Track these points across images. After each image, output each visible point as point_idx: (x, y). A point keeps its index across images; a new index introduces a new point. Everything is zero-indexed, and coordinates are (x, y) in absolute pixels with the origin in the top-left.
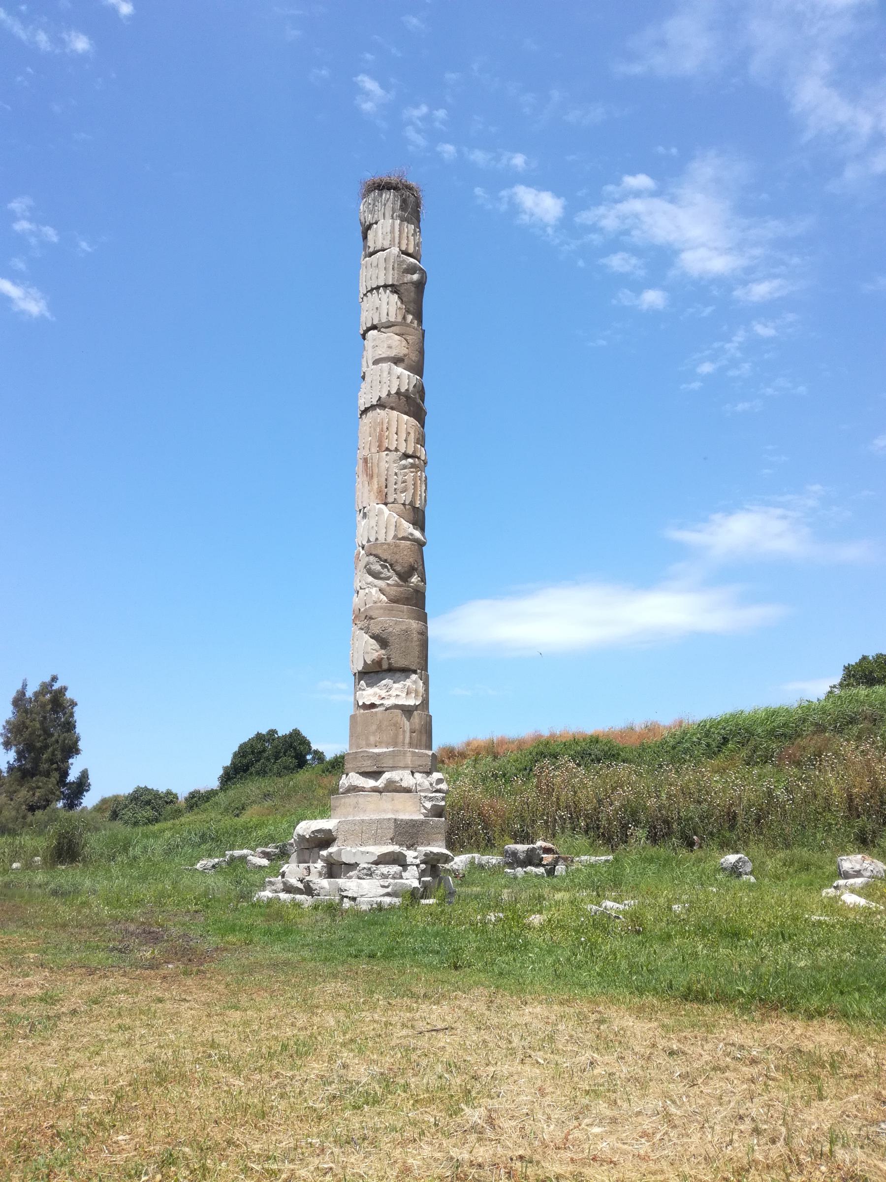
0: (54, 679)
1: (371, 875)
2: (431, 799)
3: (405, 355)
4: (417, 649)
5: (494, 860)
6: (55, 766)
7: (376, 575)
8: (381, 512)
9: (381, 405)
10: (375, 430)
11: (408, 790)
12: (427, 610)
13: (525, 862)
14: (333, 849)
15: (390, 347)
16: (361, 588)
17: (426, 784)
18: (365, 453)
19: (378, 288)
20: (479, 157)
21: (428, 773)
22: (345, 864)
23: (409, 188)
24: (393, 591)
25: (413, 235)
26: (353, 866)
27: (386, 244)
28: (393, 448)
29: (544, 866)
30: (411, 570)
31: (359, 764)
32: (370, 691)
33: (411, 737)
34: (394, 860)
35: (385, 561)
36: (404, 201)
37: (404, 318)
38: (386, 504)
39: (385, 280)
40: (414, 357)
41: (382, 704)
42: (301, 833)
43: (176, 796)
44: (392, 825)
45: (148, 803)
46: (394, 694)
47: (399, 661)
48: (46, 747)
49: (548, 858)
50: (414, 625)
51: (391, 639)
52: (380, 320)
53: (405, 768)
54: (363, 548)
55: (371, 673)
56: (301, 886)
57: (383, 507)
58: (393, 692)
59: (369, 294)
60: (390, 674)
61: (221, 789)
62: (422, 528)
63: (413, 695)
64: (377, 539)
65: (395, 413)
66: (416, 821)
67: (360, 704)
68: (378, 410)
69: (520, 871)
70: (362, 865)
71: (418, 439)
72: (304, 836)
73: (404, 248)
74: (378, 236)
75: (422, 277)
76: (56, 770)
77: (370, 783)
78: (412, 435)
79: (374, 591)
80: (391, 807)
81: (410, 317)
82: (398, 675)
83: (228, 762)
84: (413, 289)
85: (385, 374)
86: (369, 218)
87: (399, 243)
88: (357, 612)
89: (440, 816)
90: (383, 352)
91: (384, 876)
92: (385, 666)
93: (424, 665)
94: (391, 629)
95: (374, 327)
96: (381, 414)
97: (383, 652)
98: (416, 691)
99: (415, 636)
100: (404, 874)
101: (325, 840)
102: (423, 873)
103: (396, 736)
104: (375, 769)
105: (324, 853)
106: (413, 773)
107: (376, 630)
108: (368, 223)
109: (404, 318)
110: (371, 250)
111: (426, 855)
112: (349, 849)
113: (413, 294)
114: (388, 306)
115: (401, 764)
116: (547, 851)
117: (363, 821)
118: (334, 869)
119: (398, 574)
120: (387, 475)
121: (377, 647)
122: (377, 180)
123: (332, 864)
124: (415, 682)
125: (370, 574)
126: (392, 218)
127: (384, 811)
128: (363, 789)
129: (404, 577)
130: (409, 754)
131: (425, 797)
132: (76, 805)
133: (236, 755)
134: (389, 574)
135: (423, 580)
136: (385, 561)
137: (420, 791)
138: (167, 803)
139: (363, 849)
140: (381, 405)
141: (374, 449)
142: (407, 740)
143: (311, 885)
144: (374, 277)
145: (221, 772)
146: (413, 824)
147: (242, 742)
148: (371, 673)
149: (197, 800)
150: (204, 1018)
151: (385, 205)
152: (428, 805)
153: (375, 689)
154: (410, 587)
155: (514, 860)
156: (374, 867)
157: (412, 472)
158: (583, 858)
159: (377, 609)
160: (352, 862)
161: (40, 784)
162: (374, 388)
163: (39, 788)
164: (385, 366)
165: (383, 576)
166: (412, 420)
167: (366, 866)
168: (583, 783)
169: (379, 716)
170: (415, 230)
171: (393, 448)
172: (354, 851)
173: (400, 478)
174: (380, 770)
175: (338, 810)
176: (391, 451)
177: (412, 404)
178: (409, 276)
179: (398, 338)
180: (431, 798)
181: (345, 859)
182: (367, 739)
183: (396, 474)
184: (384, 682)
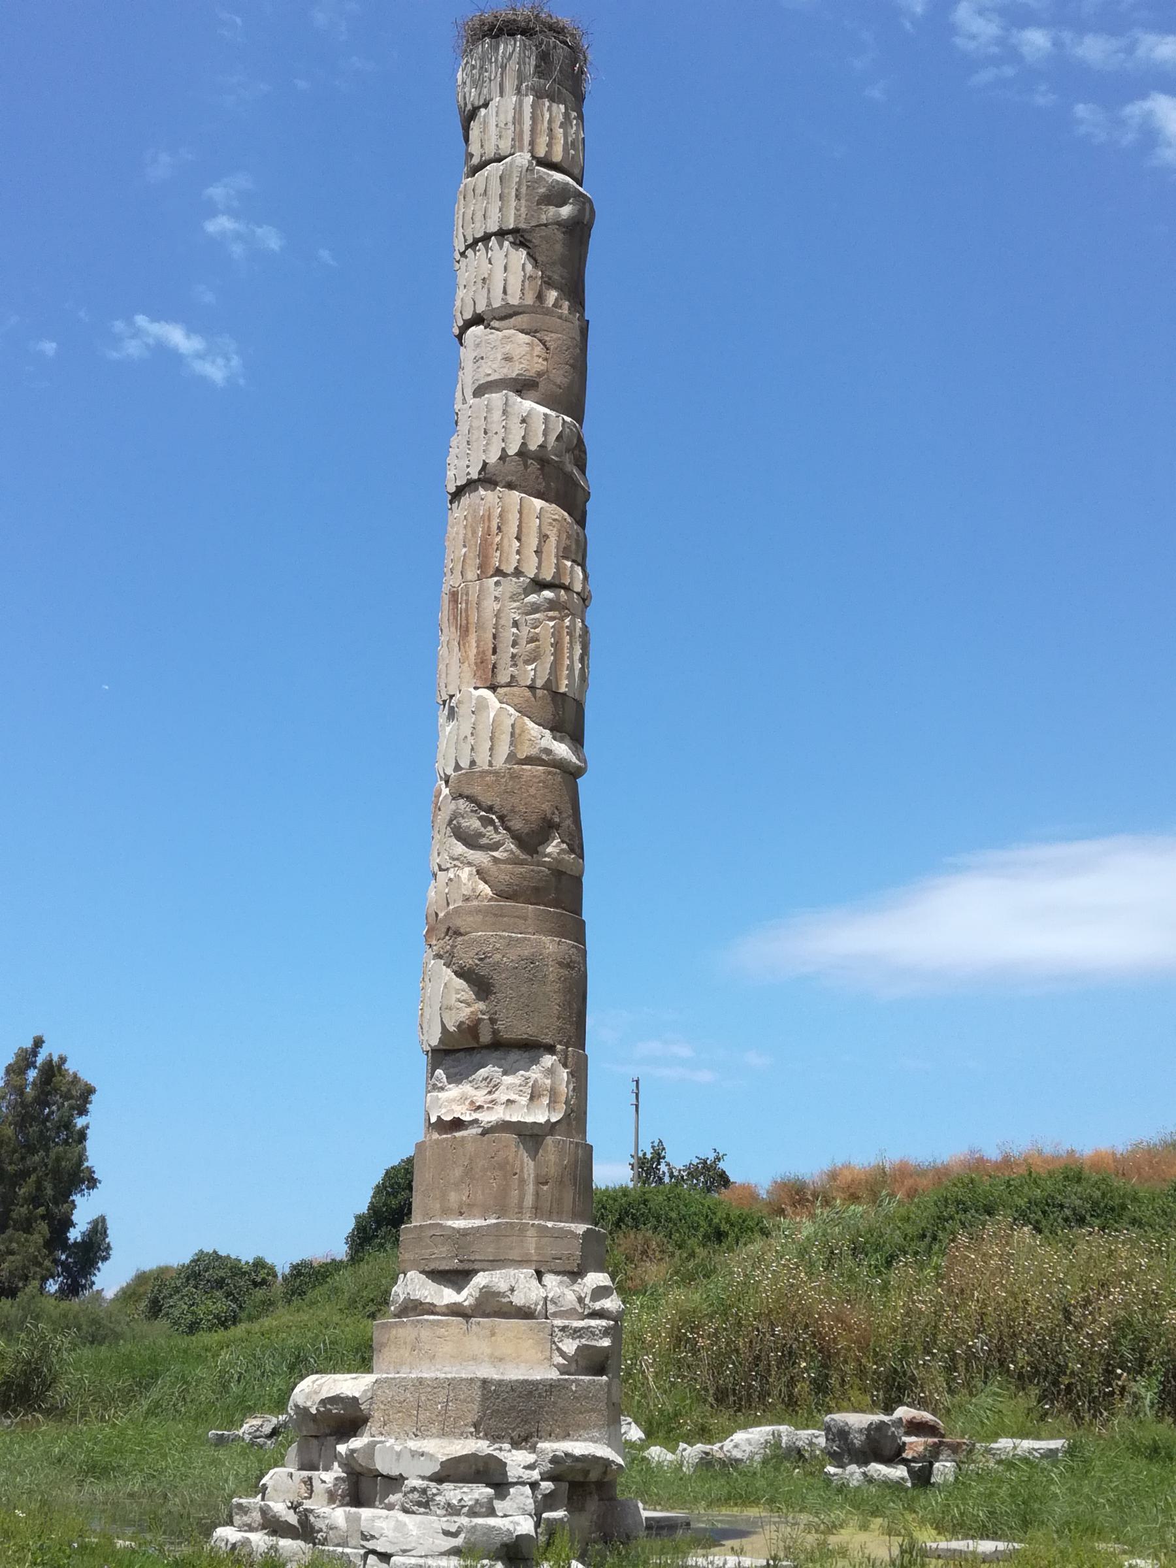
0: (38, 1043)
1: (426, 1505)
2: (576, 1333)
3: (540, 374)
4: (557, 999)
5: (812, 1437)
6: (41, 1210)
7: (470, 840)
8: (482, 705)
9: (487, 479)
10: (474, 532)
11: (525, 1313)
12: (589, 913)
13: (864, 1453)
15: (508, 359)
16: (441, 869)
17: (570, 1298)
18: (452, 581)
19: (486, 238)
20: (1093, 49)
21: (576, 1275)
22: (382, 1475)
23: (557, 30)
24: (504, 875)
25: (562, 125)
26: (395, 1482)
27: (505, 146)
28: (509, 569)
29: (905, 1462)
30: (546, 829)
31: (426, 1253)
32: (454, 1091)
33: (537, 1194)
34: (478, 1472)
35: (490, 809)
36: (544, 57)
37: (540, 297)
38: (493, 688)
39: (501, 220)
40: (560, 376)
41: (476, 1121)
42: (301, 1403)
43: (272, 1272)
44: (477, 1393)
45: (220, 1283)
46: (504, 1098)
47: (516, 1027)
48: (24, 1174)
49: (915, 1444)
50: (551, 946)
51: (498, 979)
52: (489, 304)
54: (447, 782)
55: (458, 1053)
56: (292, 1519)
58: (502, 1096)
59: (470, 252)
60: (497, 1054)
61: (352, 1258)
62: (576, 738)
63: (545, 1101)
64: (473, 763)
65: (516, 495)
66: (535, 1384)
67: (433, 1120)
68: (482, 492)
69: (854, 1472)
71: (566, 548)
72: (306, 1409)
73: (541, 152)
74: (491, 132)
75: (582, 211)
76: (43, 1217)
77: (448, 1296)
78: (553, 540)
79: (465, 873)
80: (488, 1351)
81: (552, 295)
82: (514, 1055)
83: (363, 1208)
84: (560, 236)
85: (497, 415)
86: (473, 95)
87: (532, 143)
88: (432, 919)
89: (601, 1371)
90: (494, 370)
91: (453, 1510)
92: (485, 1037)
93: (577, 1036)
94: (498, 957)
95: (477, 320)
96: (487, 497)
97: (481, 1005)
98: (553, 1093)
99: (552, 971)
100: (498, 1504)
101: (346, 1420)
102: (548, 1502)
103: (504, 1192)
104: (455, 1264)
105: (342, 1448)
106: (539, 1275)
107: (468, 959)
108: (469, 107)
109: (540, 297)
110: (475, 161)
111: (555, 1460)
112: (391, 1441)
113: (563, 249)
114: (507, 273)
115: (515, 1255)
116: (916, 1428)
117: (421, 1381)
118: (363, 1486)
119: (517, 838)
120: (496, 626)
121: (469, 995)
122: (488, 16)
123: (360, 1474)
124: (550, 1072)
125: (459, 838)
126: (518, 91)
127: (474, 1359)
128: (431, 1309)
129: (530, 842)
130: (531, 1232)
131: (563, 1329)
132: (84, 1287)
133: (379, 1190)
134: (497, 838)
135: (576, 846)
136: (490, 809)
137: (555, 1315)
138: (255, 1284)
139: (413, 1444)
140: (487, 479)
141: (471, 574)
142: (529, 1201)
143: (312, 1519)
144: (479, 216)
145: (350, 1225)
146: (528, 1390)
147: (388, 1166)
148: (458, 1053)
149: (307, 1278)
151: (504, 67)
152: (570, 1346)
153: (466, 1088)
154: (544, 864)
155: (846, 1449)
157: (551, 619)
158: (1004, 1443)
159: (470, 913)
160: (394, 1472)
161: (14, 1245)
162: (474, 445)
163: (12, 1253)
165: (484, 841)
166: (555, 511)
168: (1020, 1268)
169: (470, 1148)
170: (566, 115)
171: (509, 569)
172: (398, 1448)
173: (525, 632)
174: (467, 1266)
175: (385, 1350)
176: (505, 575)
177: (557, 475)
178: (552, 210)
179: (527, 338)
181: (383, 1465)
182: (444, 1197)
183: (516, 624)
184: (483, 1072)
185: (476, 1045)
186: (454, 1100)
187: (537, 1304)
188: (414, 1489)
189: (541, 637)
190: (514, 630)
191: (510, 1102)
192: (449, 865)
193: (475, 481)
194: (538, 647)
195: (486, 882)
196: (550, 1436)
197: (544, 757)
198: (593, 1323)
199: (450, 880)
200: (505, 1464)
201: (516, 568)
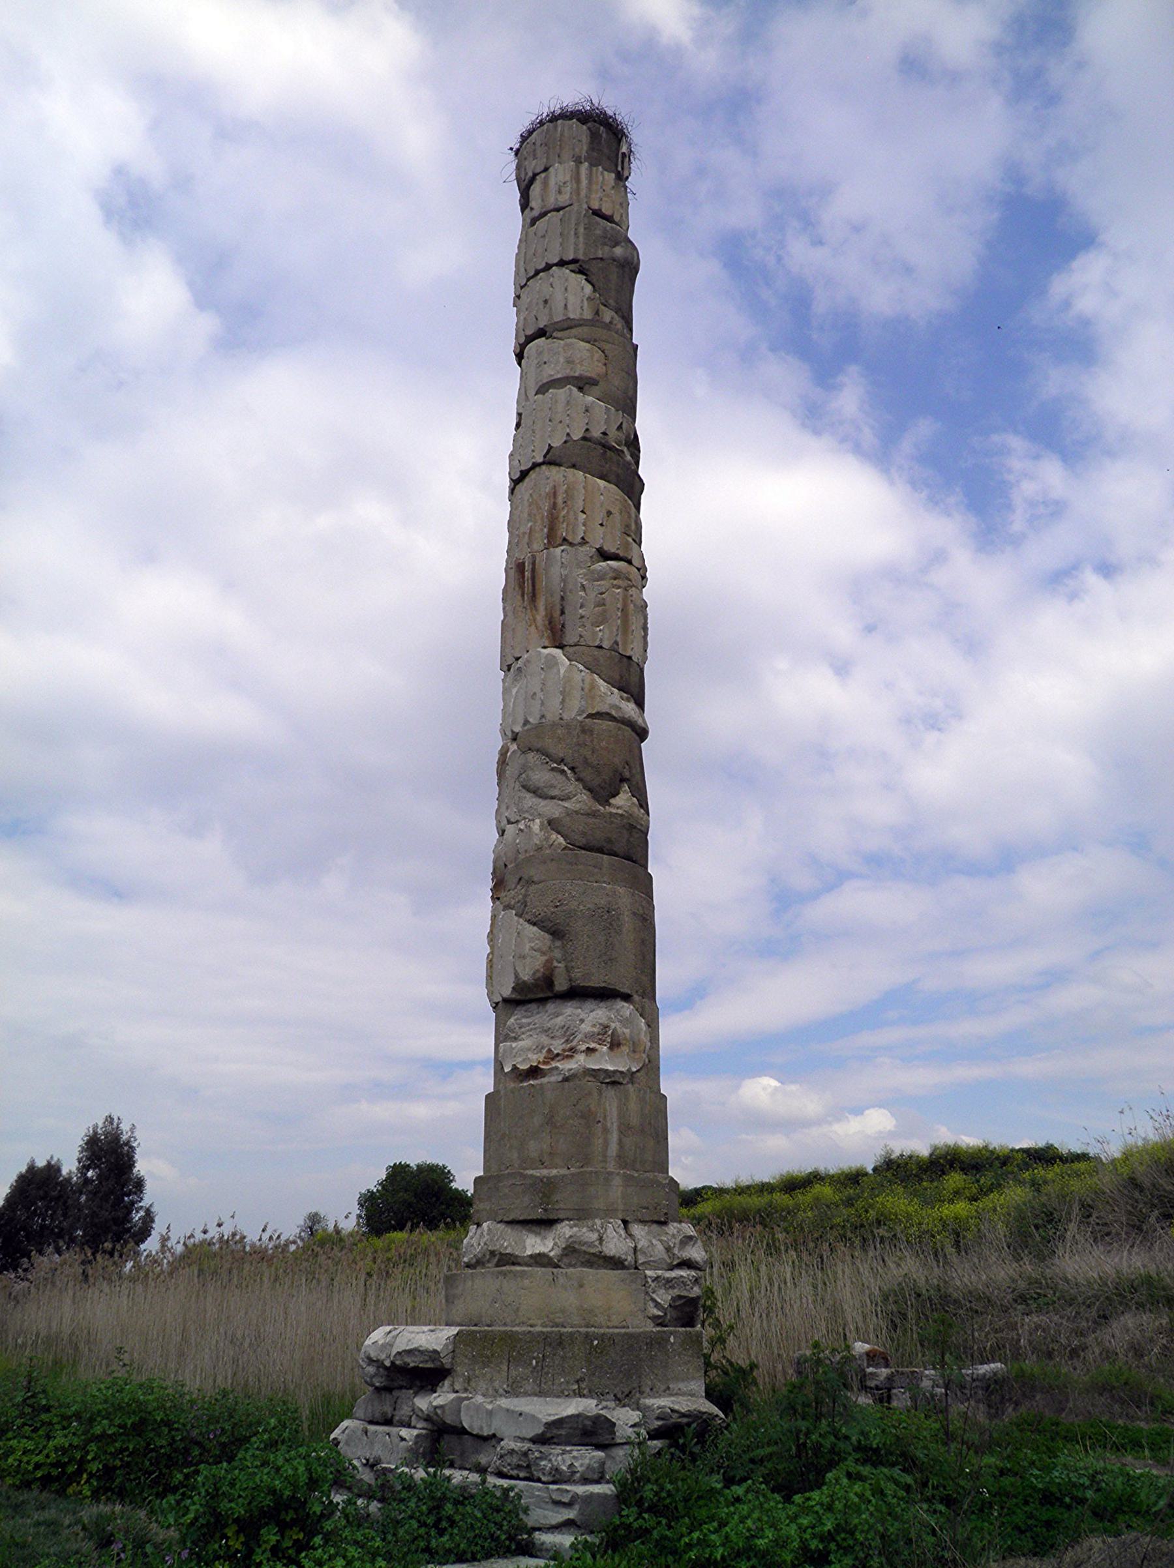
8: (552, 663)
11: (615, 1263)
14: (441, 1398)
16: (509, 822)
19: (548, 267)
33: (620, 1142)
53: (609, 1213)
56: (367, 1476)
57: (557, 652)
70: (509, 1444)
77: (535, 1244)
85: (560, 407)
104: (539, 1213)
105: (423, 1403)
108: (530, 174)
130: (617, 1181)
131: (657, 1279)
135: (644, 805)
142: (613, 1149)
150: (594, 971)
152: (664, 1297)
156: (536, 1451)
164: (561, 394)
167: (513, 1445)
171: (578, 540)
179: (588, 346)
180: (668, 1281)
185: (550, 994)
186: (529, 1050)
187: (626, 1254)
188: (512, 1452)
189: (608, 602)
190: (582, 593)
191: (590, 1050)
192: (518, 818)
193: (539, 465)
194: (605, 611)
195: (559, 833)
196: (654, 1392)
197: (613, 713)
198: (683, 1273)
199: (521, 830)
200: (614, 1424)
201: (583, 538)
